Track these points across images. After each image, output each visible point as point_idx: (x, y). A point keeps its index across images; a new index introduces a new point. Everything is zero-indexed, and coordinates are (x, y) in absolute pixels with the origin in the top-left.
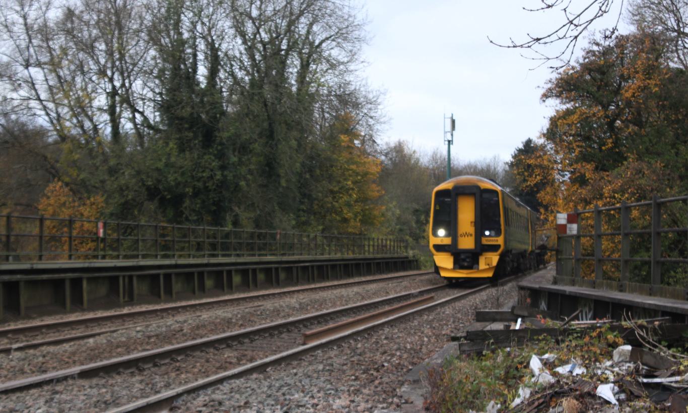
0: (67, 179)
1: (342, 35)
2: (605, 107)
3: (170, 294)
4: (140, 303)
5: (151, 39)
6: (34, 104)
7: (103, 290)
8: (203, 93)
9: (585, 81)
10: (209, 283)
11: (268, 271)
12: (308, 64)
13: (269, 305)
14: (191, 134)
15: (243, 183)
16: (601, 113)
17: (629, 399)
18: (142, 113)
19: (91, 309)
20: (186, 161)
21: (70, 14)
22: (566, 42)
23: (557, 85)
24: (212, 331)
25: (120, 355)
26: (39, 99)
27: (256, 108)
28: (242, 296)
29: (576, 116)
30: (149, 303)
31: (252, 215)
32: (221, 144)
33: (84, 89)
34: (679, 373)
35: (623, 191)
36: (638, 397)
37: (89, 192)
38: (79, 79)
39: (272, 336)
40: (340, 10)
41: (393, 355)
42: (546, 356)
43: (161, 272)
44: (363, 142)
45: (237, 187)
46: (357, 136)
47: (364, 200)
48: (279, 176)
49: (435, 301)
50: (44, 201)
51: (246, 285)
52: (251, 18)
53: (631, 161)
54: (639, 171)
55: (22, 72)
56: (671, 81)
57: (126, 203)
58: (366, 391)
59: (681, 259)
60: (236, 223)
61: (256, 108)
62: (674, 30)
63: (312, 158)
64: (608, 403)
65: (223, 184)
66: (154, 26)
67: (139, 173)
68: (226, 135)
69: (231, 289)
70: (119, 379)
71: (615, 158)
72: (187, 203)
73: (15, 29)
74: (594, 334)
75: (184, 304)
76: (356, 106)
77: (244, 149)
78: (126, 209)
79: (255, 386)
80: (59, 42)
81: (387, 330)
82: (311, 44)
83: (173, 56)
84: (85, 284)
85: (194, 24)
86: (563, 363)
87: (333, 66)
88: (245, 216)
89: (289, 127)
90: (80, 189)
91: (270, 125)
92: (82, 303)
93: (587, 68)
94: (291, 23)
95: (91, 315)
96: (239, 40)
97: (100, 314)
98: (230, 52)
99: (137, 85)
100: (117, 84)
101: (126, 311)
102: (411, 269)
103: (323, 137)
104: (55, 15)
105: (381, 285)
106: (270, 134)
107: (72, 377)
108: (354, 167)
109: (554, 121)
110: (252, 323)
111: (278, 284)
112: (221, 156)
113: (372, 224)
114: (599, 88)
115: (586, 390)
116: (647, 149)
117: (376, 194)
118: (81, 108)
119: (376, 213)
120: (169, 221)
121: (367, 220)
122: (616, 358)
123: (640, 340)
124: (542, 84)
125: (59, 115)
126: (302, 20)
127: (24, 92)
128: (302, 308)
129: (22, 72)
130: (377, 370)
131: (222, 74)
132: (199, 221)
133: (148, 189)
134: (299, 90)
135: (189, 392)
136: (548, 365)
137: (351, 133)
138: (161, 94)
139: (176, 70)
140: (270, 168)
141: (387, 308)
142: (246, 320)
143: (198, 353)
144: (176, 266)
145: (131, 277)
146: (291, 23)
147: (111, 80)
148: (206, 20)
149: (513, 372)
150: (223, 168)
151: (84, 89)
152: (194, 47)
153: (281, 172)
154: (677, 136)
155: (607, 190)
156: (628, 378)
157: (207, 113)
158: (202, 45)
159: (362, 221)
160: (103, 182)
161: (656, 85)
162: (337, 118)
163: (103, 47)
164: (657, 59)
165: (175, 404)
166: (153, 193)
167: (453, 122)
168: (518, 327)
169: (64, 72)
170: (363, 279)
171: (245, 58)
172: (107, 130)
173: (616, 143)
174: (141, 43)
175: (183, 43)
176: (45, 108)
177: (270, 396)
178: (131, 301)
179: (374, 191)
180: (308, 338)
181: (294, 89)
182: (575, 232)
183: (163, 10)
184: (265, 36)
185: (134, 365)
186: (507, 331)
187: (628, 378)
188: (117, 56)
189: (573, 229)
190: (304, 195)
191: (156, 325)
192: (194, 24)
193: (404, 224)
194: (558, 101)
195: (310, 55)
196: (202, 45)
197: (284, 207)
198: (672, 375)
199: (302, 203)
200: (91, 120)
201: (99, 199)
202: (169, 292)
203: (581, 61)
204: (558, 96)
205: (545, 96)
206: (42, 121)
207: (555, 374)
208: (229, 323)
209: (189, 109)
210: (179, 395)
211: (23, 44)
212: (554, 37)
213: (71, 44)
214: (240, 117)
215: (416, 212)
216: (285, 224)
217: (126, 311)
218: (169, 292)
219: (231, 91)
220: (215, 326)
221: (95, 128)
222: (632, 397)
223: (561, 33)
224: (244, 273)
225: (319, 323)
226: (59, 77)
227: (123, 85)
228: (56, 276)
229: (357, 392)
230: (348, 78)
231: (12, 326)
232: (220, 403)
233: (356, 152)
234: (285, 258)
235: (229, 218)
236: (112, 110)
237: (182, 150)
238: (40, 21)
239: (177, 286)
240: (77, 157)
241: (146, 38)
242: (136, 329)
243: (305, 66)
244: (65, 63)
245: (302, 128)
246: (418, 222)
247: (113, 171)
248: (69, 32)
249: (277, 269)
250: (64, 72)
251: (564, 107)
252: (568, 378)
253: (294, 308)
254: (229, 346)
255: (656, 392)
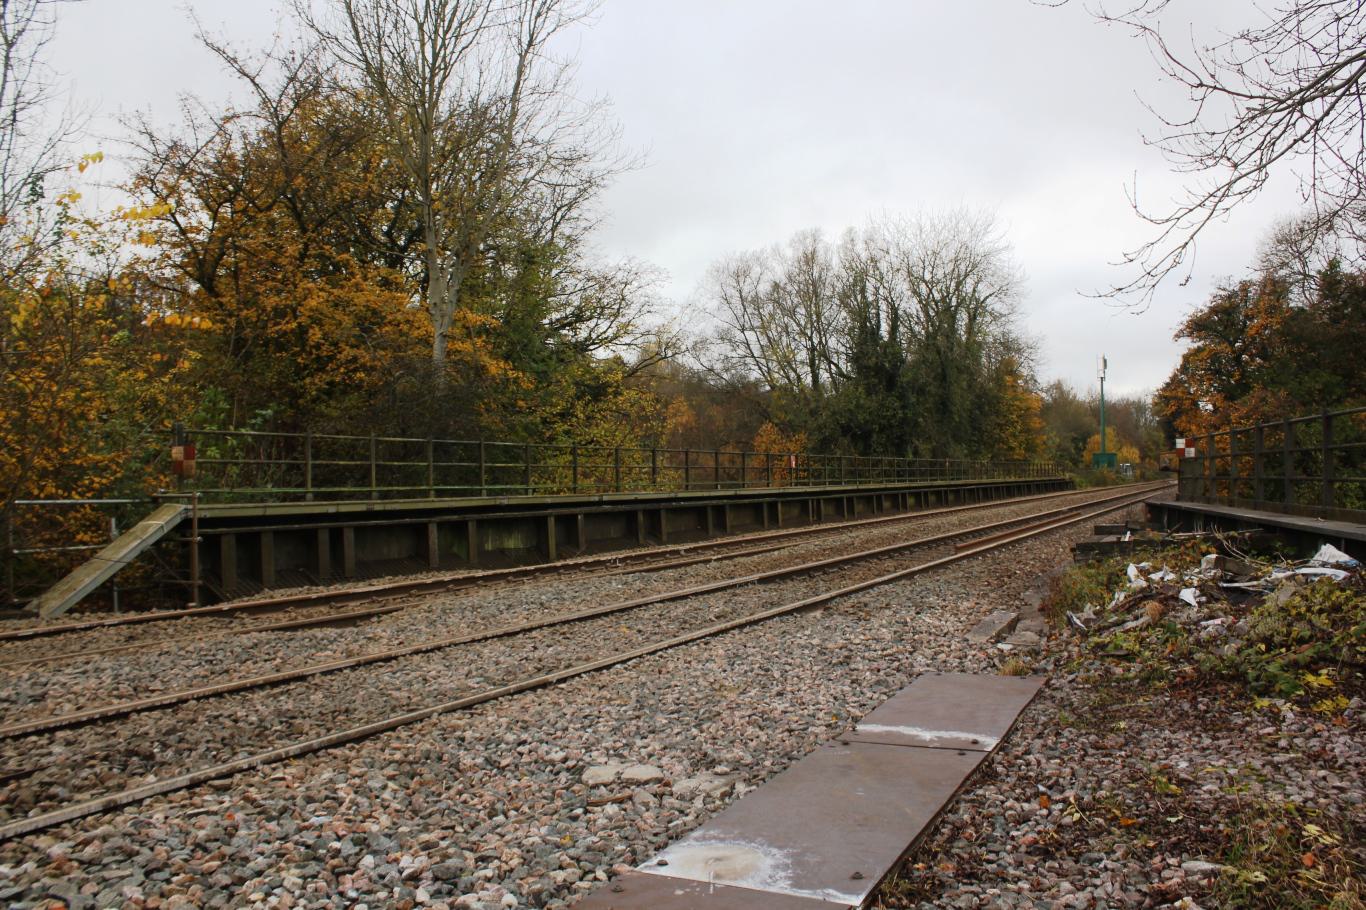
0: (776, 421)
1: (1001, 292)
2: (1232, 344)
3: (852, 515)
4: (825, 522)
5: (842, 302)
6: (749, 360)
7: (795, 511)
8: (886, 346)
9: (1214, 321)
10: (886, 504)
11: (938, 494)
12: (975, 318)
13: (932, 522)
14: (876, 381)
15: (921, 420)
16: (1229, 349)
17: (1208, 602)
18: (836, 366)
19: (786, 527)
20: (872, 403)
21: (776, 286)
22: (1146, 289)
23: (1188, 327)
24: (879, 545)
25: (797, 564)
26: (753, 356)
27: (931, 356)
28: (915, 514)
29: (1205, 353)
30: (834, 522)
31: (929, 447)
32: (902, 387)
33: (788, 346)
34: (1257, 578)
35: (1248, 417)
36: (1217, 600)
37: (794, 431)
38: (784, 339)
39: (930, 548)
40: (1001, 270)
41: (1026, 564)
42: (1143, 564)
43: (844, 495)
44: (1026, 382)
45: (917, 424)
46: (1020, 377)
47: (1027, 431)
48: (951, 412)
49: (1286, 512)
50: (758, 439)
51: (918, 506)
52: (924, 281)
53: (1257, 391)
54: (1263, 399)
55: (739, 336)
56: (1292, 318)
57: (825, 439)
58: (992, 595)
59: (1304, 477)
60: (916, 453)
61: (931, 356)
62: (1300, 273)
63: (979, 397)
64: (1189, 605)
65: (904, 421)
66: (844, 293)
67: (834, 413)
68: (905, 379)
69: (905, 509)
70: (790, 584)
71: (1244, 387)
72: (875, 436)
73: (733, 301)
74: (1189, 545)
75: (864, 522)
76: (1019, 351)
77: (921, 391)
78: (824, 445)
79: (899, 591)
80: (768, 308)
81: (1030, 542)
82: (977, 300)
83: (860, 316)
84: (779, 506)
85: (877, 289)
86: (1156, 569)
87: (995, 318)
88: (923, 447)
89: (960, 371)
90: (787, 429)
91: (943, 370)
92: (725, 528)
93: (1214, 310)
94: (959, 284)
95: (784, 532)
96: (915, 300)
97: (792, 531)
98: (908, 310)
99: (832, 342)
100: (816, 341)
101: (813, 528)
102: (1067, 489)
103: (991, 379)
104: (764, 288)
105: (1035, 503)
106: (943, 378)
107: (753, 583)
108: (1017, 403)
109: (1186, 358)
110: (915, 537)
111: (947, 504)
112: (901, 397)
113: (1035, 451)
114: (1226, 328)
115: (1170, 593)
116: (1272, 380)
117: (1038, 425)
118: (787, 363)
119: (1038, 441)
120: (860, 455)
121: (1031, 448)
122: (1204, 565)
123: (524, 568)
124: (1174, 326)
125: (769, 369)
126: (968, 280)
127: (742, 351)
128: (961, 524)
129: (739, 336)
130: (1009, 577)
131: (902, 329)
132: (884, 453)
133: (842, 427)
134: (968, 339)
135: (841, 595)
136: (1144, 573)
137: (1014, 374)
138: (851, 348)
139: (863, 327)
140: (944, 406)
141: (1038, 523)
142: (911, 534)
143: (863, 563)
144: (858, 491)
145: (818, 501)
146: (959, 284)
147: (811, 339)
148: (886, 285)
149: (1114, 578)
150: (904, 407)
151: (788, 346)
152: (878, 308)
153: (954, 409)
154: (1300, 367)
155: (1234, 416)
156: (1211, 583)
157: (889, 362)
158: (883, 306)
159: (1025, 449)
160: (806, 422)
161: (1278, 323)
162: (1001, 362)
163: (803, 311)
164: (1278, 300)
165: (829, 605)
166: (846, 430)
167: (1105, 361)
168: (1127, 540)
169: (773, 334)
170: (1023, 499)
171: (922, 315)
172: (808, 380)
173: (1243, 375)
174: (834, 307)
175: (868, 305)
176: (758, 363)
177: (909, 599)
178: (819, 521)
179: (1036, 423)
180: (958, 550)
181: (964, 338)
182: (1193, 455)
183: (851, 280)
184: (937, 296)
185: (807, 572)
186: (1119, 542)
187: (1211, 583)
188: (814, 317)
189: (1191, 452)
190: (974, 429)
191: (832, 540)
192: (877, 289)
193: (1064, 450)
194: (1189, 340)
195: (976, 309)
196: (883, 306)
197: (957, 439)
198: (1250, 580)
199: (974, 435)
200: (795, 371)
201: (803, 436)
202: (851, 511)
203: (1209, 305)
204: (1190, 335)
205: (1178, 336)
206: (755, 375)
207: (1148, 580)
208: (895, 538)
209: (874, 359)
210: (833, 598)
211: (740, 313)
212: (1134, 287)
213: (778, 311)
214: (916, 364)
215: (1074, 440)
216: (959, 453)
217: (813, 528)
218: (851, 511)
219: (910, 343)
220: (882, 541)
221: (799, 377)
222: (1212, 599)
223: (1140, 284)
224: (917, 496)
225: (974, 537)
226: (769, 338)
227: (820, 342)
228: (756, 500)
229: (985, 595)
230: (1010, 327)
231: (719, 541)
232: (866, 605)
233: (1020, 390)
234: (953, 483)
235: (910, 450)
236: (812, 364)
237: (869, 393)
238: (753, 294)
239: (858, 507)
240: (784, 402)
241: (838, 302)
242: (814, 544)
243: (972, 318)
244: (773, 326)
245: (972, 373)
246: (1076, 448)
247: (813, 413)
248: (776, 301)
249: (946, 492)
250: (773, 334)
251: (1196, 345)
252: (1158, 583)
253: (953, 525)
254: (891, 557)
255: (1234, 595)
